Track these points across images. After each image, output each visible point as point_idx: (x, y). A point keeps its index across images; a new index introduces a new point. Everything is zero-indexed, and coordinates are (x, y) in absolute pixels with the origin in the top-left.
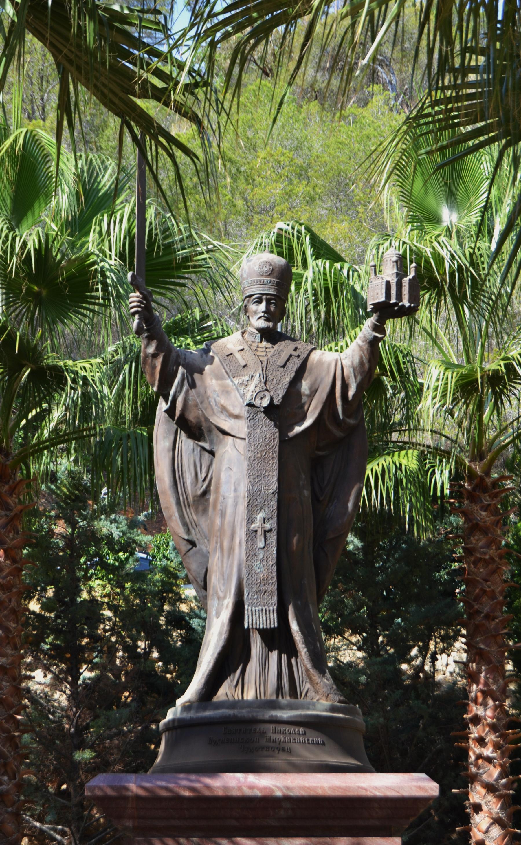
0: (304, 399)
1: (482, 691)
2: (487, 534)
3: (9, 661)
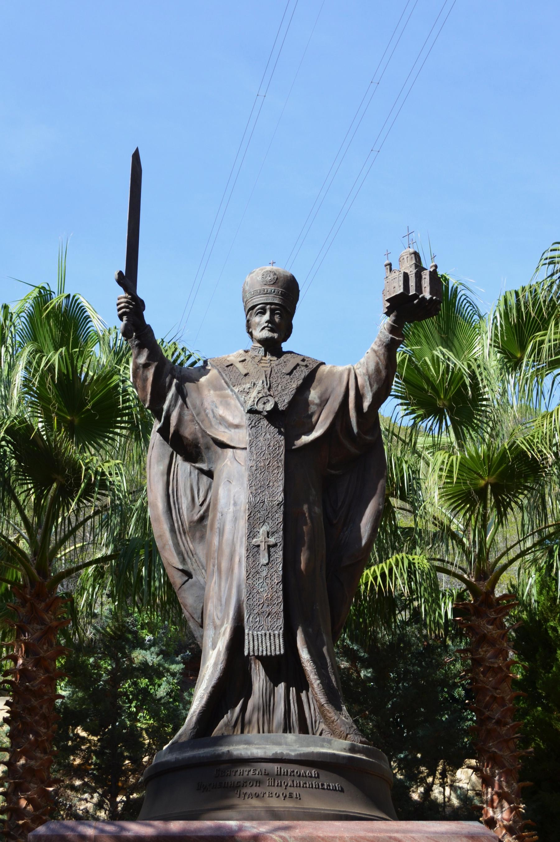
0: (313, 408)
1: (497, 793)
2: (495, 646)
3: (38, 764)
